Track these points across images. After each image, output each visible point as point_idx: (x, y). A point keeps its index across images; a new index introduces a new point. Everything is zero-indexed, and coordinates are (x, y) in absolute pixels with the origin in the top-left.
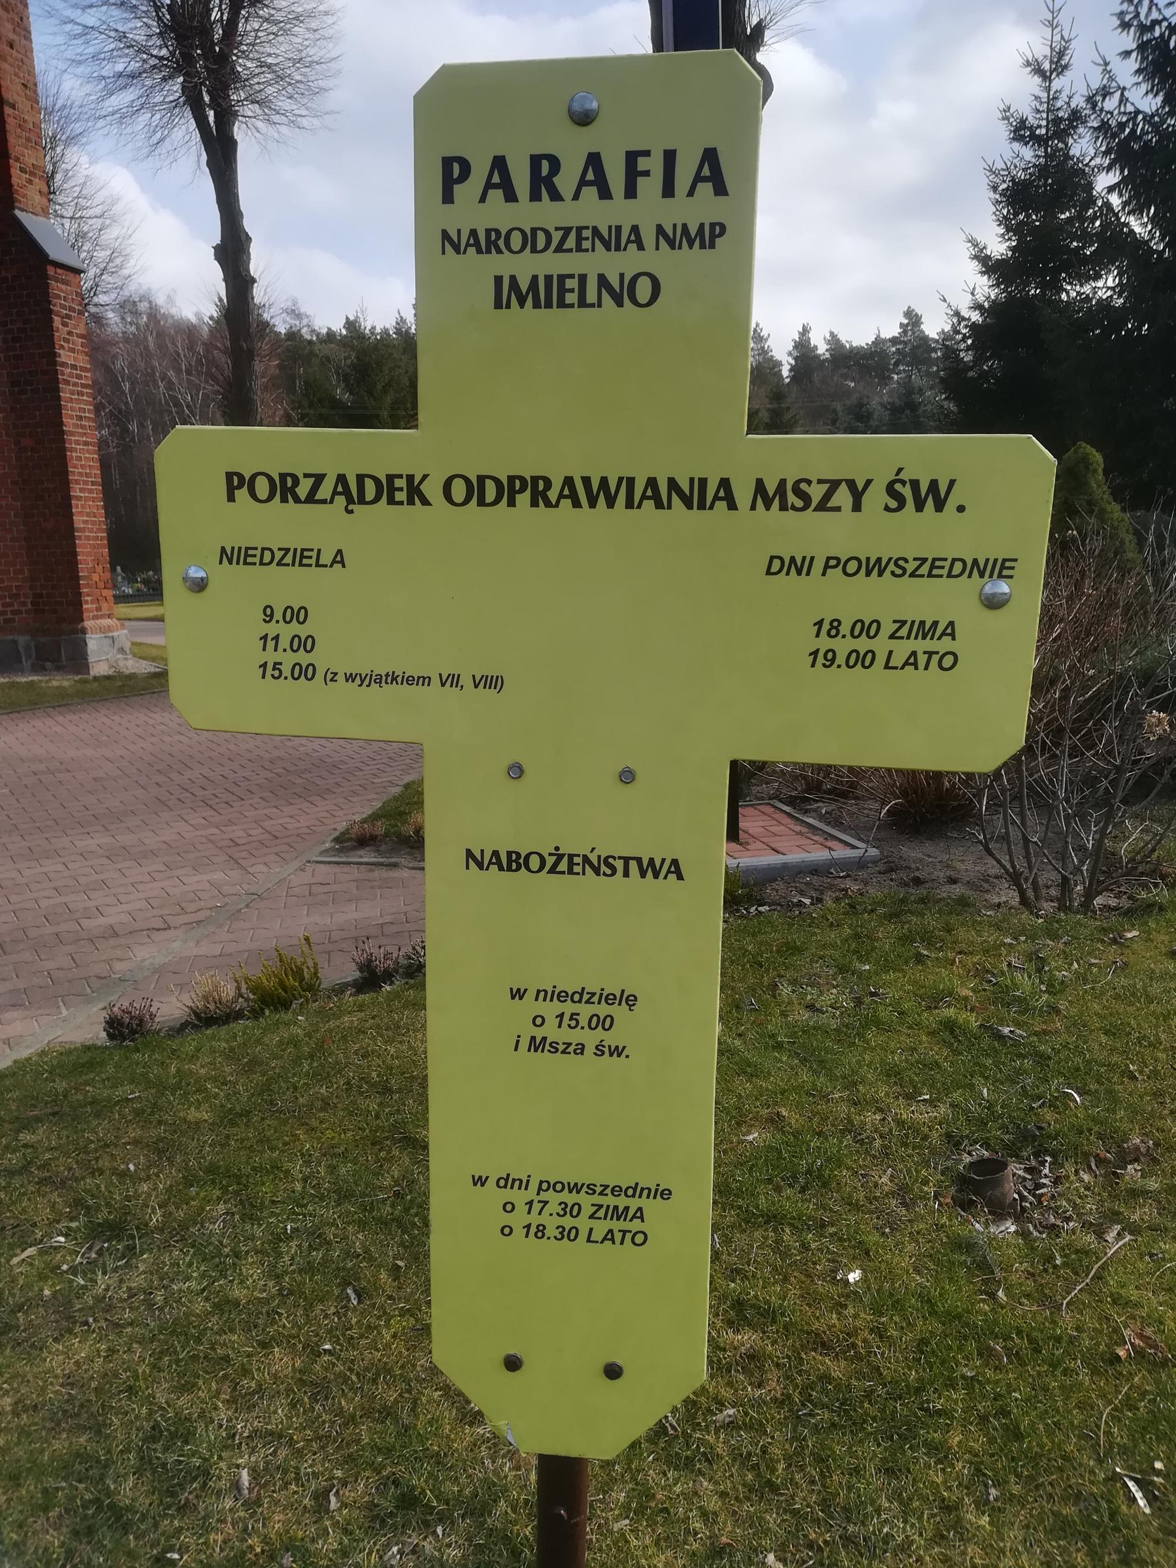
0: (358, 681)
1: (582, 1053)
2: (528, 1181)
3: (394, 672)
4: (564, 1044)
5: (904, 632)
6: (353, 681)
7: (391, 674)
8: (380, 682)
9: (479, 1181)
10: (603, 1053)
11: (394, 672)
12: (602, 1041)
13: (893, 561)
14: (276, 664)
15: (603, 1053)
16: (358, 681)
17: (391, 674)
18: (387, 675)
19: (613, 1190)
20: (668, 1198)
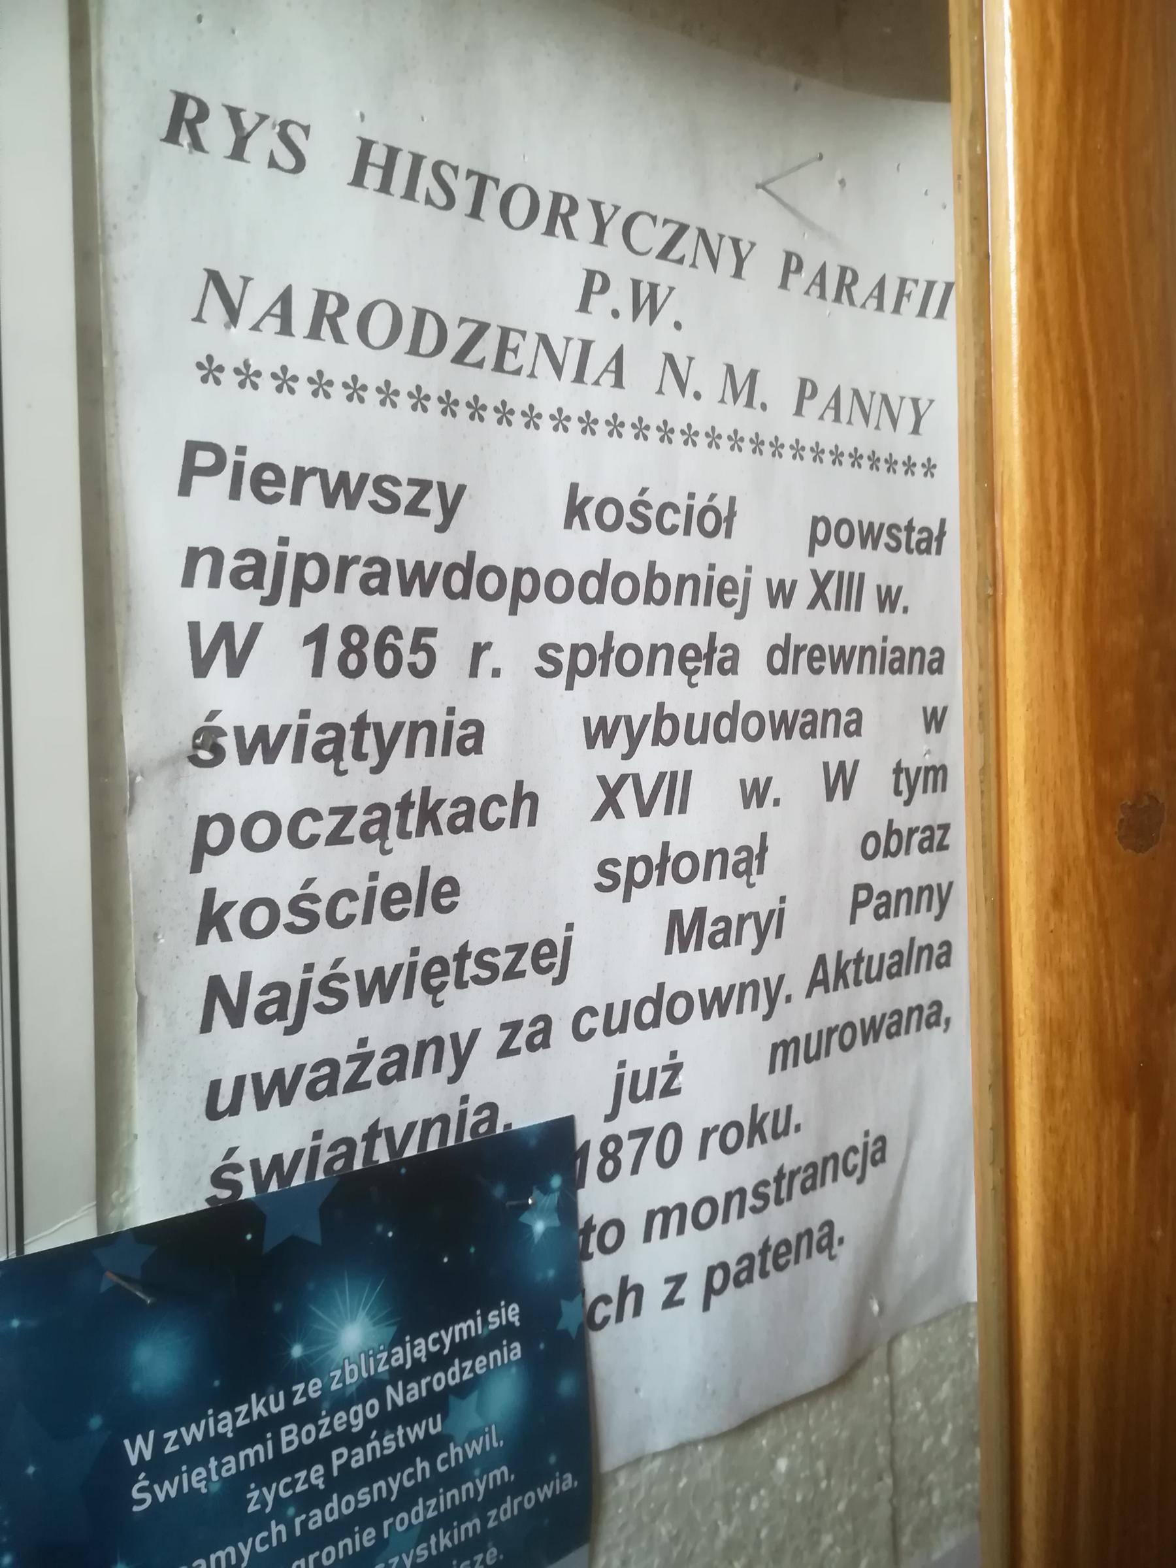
0: (621, 741)
1: (477, 749)
2: (568, 941)
3: (426, 791)
4: (411, 482)
5: (662, 1079)
6: (608, 743)
7: (416, 797)
8: (337, 756)
9: (570, 927)
10: (343, 998)
11: (426, 791)
12: (309, 882)
13: (369, 485)
14: (421, 633)
15: (343, 998)
16: (621, 741)
17: (416, 797)
18: (405, 805)
19: (536, 957)
20: (454, 905)
